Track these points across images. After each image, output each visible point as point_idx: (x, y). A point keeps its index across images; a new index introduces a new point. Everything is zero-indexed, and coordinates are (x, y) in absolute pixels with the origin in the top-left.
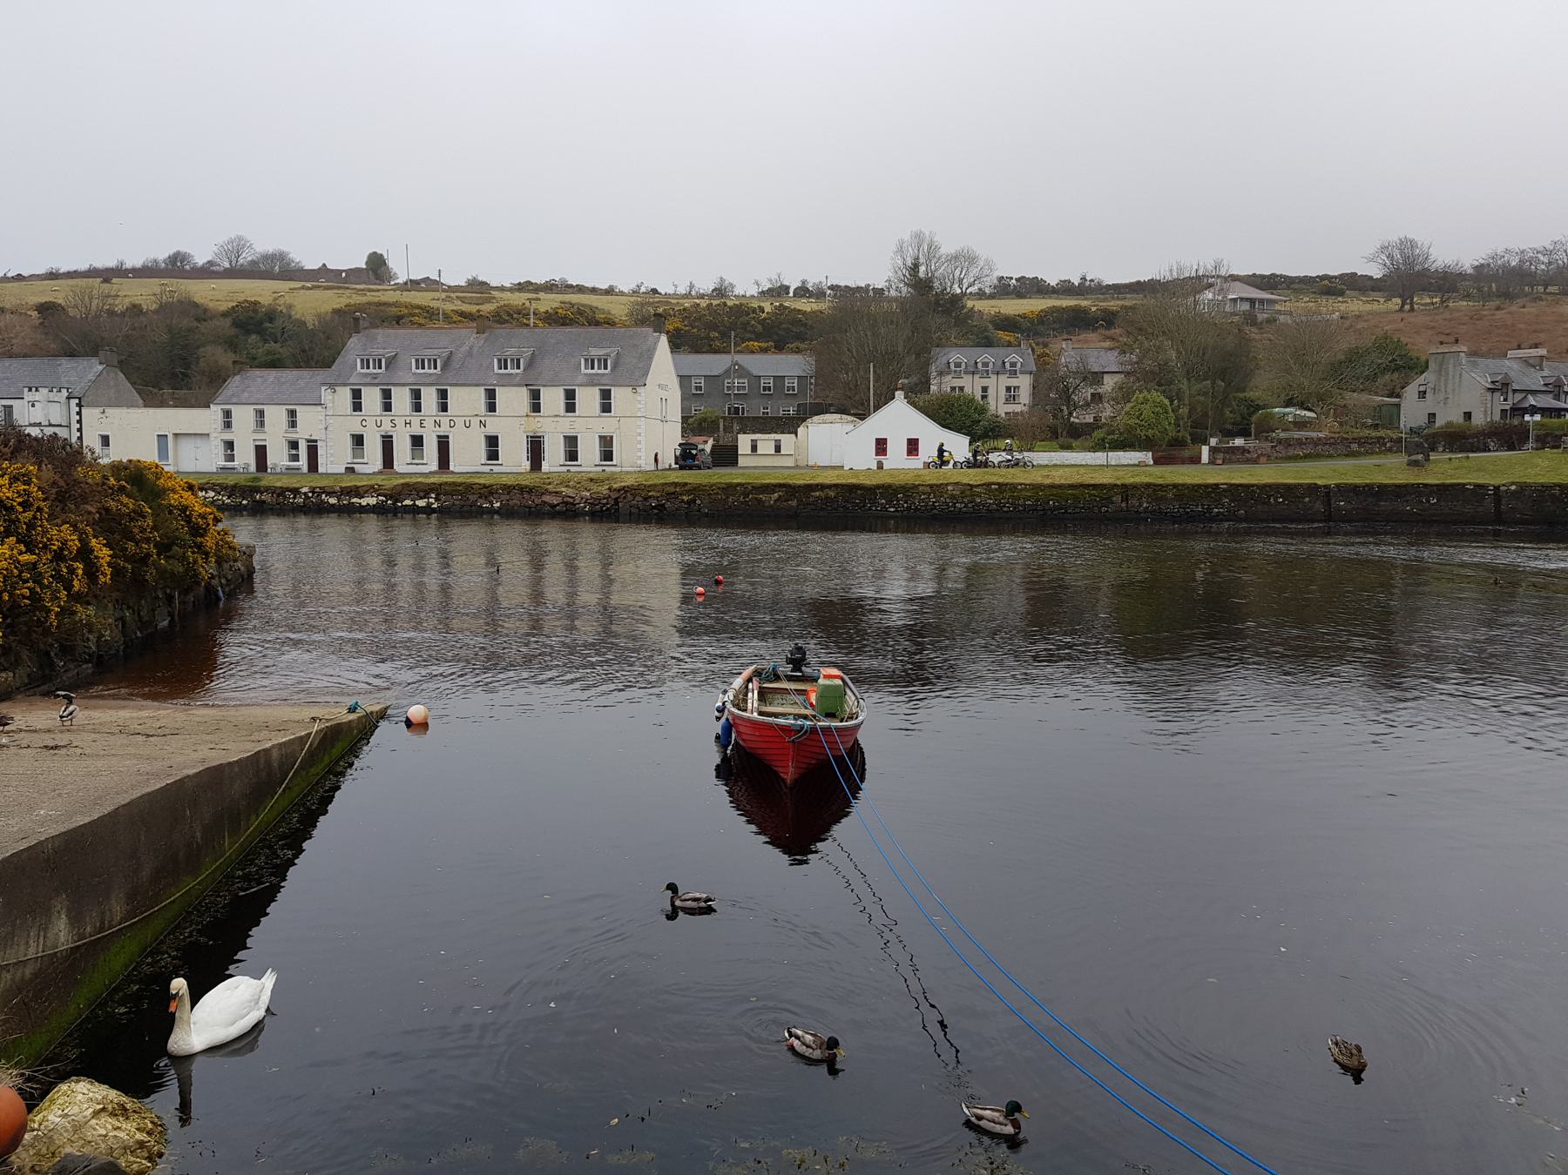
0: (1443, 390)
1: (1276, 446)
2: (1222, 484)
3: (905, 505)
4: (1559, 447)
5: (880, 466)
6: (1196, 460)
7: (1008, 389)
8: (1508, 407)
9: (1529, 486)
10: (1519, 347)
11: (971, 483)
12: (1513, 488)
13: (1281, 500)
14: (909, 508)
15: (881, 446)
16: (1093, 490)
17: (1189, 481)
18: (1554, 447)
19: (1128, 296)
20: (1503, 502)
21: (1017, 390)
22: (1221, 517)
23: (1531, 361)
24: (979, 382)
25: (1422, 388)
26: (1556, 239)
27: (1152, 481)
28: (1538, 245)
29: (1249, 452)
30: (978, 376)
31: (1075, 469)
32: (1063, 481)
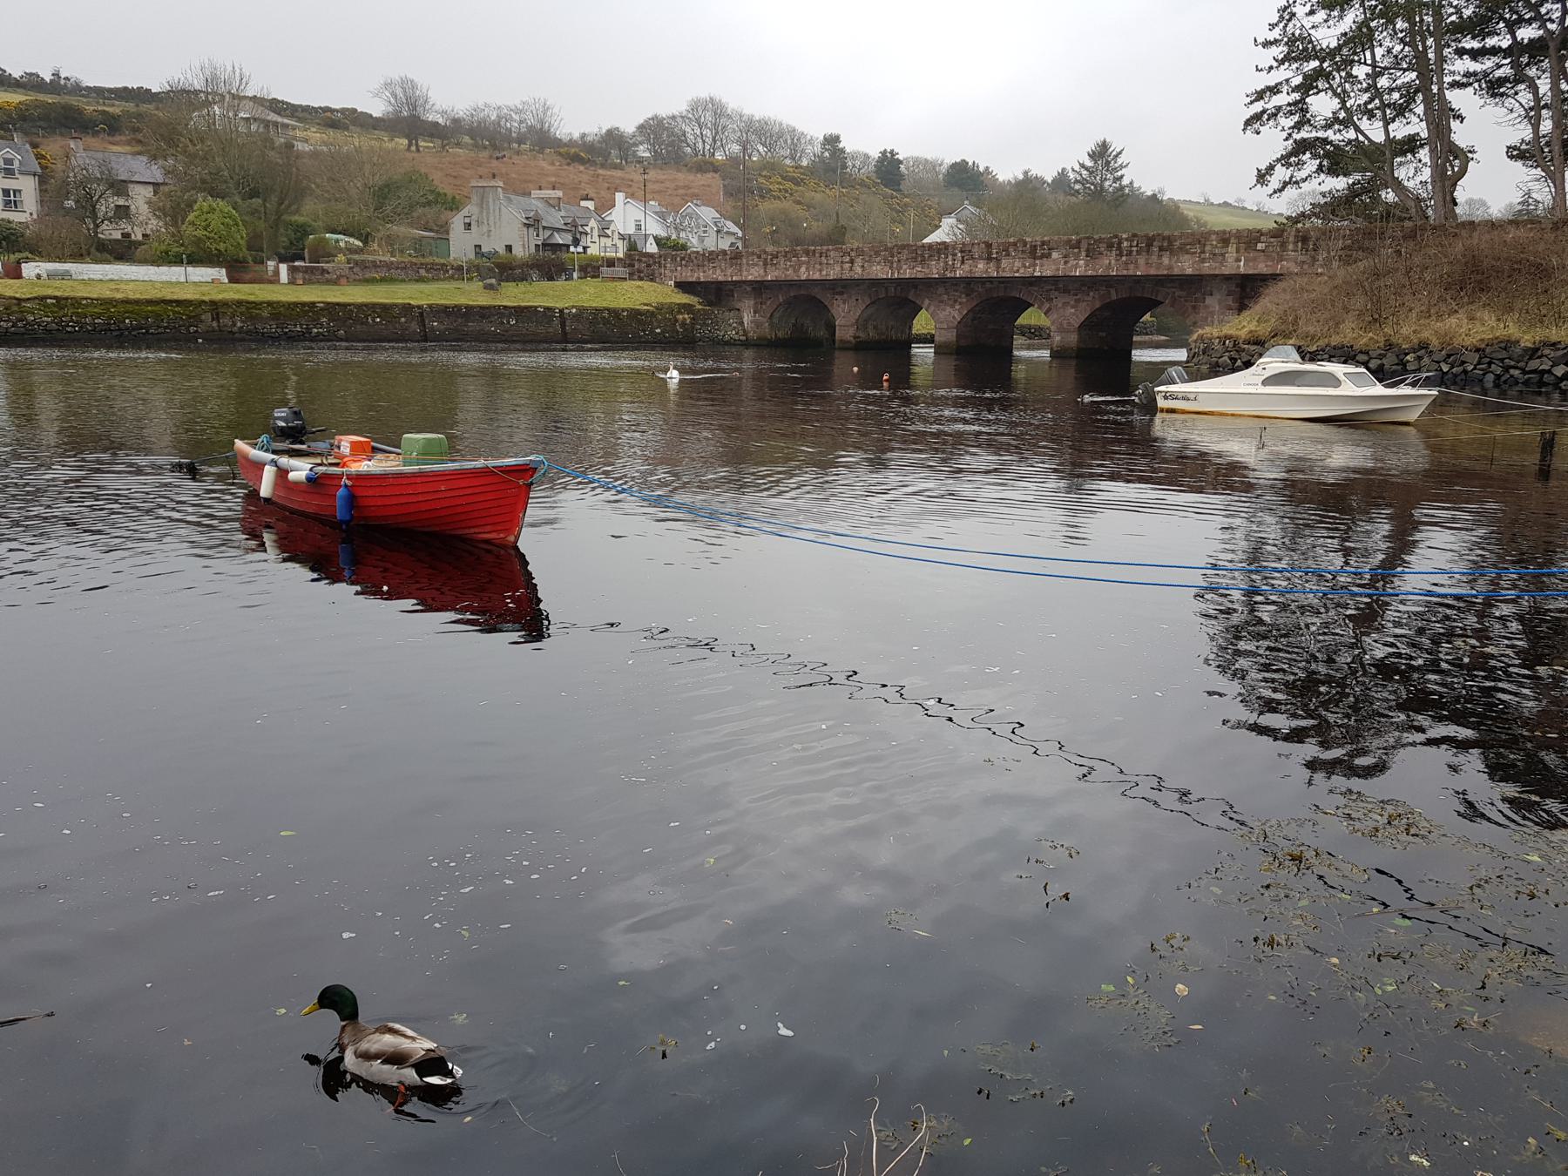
0: (485, 222)
1: (353, 268)
2: (319, 303)
4: (598, 276)
6: (275, 279)
8: (540, 243)
9: (585, 309)
10: (540, 188)
11: (17, 296)
12: (574, 311)
13: (378, 320)
16: (177, 306)
17: (283, 299)
18: (593, 277)
23: (551, 202)
25: (467, 220)
26: (524, 100)
27: (243, 297)
28: (511, 103)
29: (328, 273)
32: (138, 296)
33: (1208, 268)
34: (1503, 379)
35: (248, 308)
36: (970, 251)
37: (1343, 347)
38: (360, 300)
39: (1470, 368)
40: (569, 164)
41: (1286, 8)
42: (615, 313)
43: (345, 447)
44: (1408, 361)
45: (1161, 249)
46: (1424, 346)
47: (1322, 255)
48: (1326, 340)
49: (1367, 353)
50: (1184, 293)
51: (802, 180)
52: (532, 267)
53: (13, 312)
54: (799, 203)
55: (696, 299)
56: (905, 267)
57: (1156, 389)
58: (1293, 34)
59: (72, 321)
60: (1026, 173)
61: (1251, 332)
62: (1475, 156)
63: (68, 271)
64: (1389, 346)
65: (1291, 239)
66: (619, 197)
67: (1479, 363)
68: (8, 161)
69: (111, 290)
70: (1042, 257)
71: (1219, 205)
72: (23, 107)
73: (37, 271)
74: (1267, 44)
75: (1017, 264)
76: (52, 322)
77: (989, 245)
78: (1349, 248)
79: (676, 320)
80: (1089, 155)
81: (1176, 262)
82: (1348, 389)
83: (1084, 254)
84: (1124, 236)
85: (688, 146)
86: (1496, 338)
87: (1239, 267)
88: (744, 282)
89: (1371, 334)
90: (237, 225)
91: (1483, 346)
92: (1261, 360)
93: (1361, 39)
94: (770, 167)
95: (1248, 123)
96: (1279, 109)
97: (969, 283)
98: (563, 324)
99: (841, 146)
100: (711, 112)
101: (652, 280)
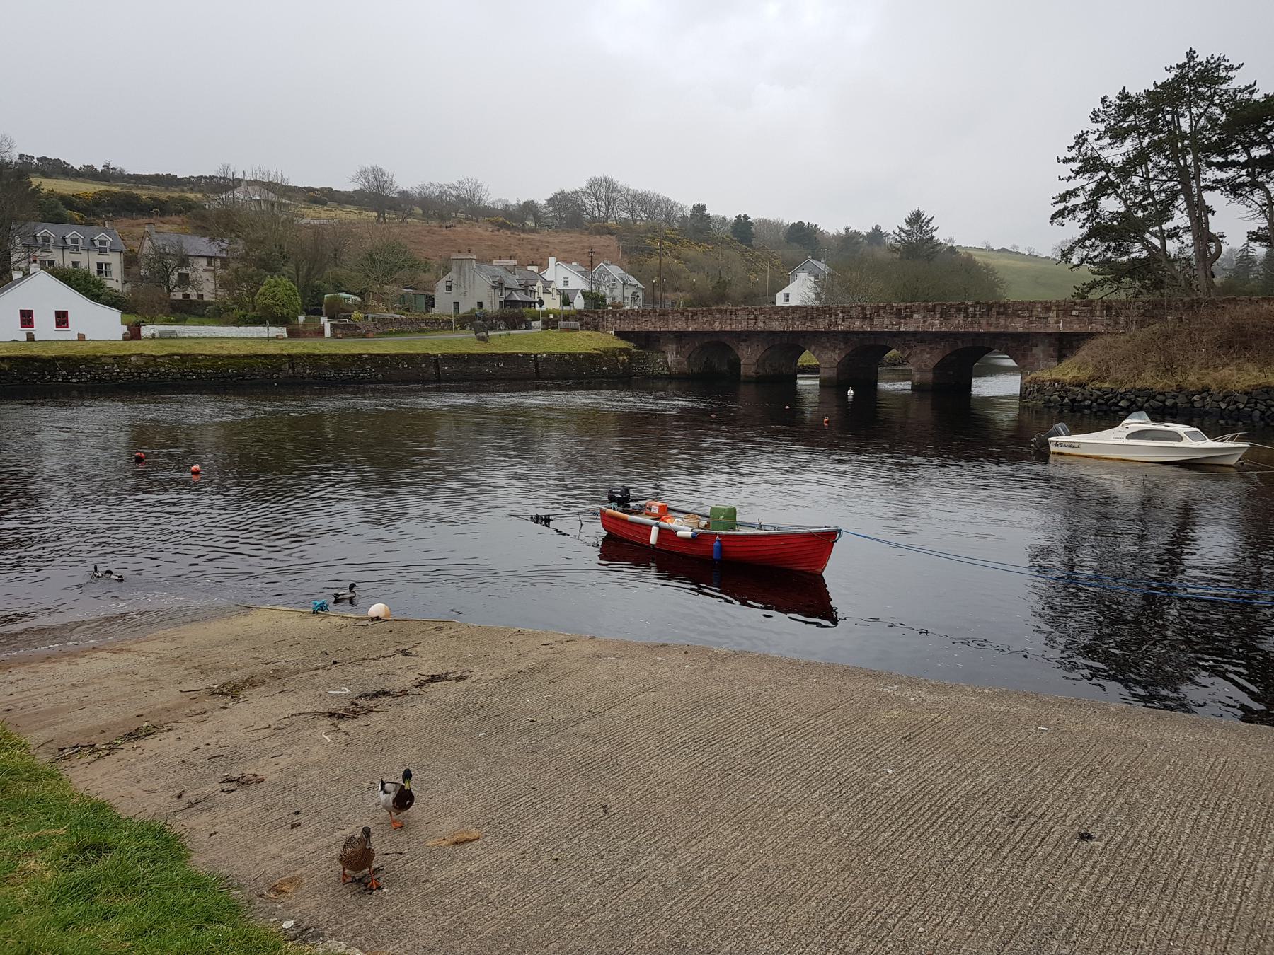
3: (89, 376)
4: (557, 328)
5: (30, 337)
6: (320, 333)
7: (100, 265)
8: (502, 300)
11: (153, 354)
14: (93, 379)
15: (27, 318)
18: (552, 328)
19: (151, 187)
20: (540, 364)
21: (108, 266)
22: (366, 380)
24: (95, 258)
25: (448, 284)
27: (311, 352)
30: (69, 251)
31: (243, 341)
32: (237, 352)
33: (1035, 327)
34: (1266, 415)
35: (315, 360)
36: (849, 312)
37: (1145, 389)
38: (393, 352)
39: (1242, 406)
40: (498, 230)
41: (1080, 136)
42: (573, 356)
43: (655, 509)
44: (1195, 401)
45: (998, 313)
46: (1206, 389)
47: (1122, 320)
48: (1132, 384)
49: (1163, 394)
50: (1015, 344)
51: (678, 240)
52: (498, 319)
53: (150, 366)
54: (677, 258)
55: (632, 344)
56: (797, 323)
57: (1050, 439)
58: (1086, 154)
59: (191, 372)
60: (847, 229)
61: (1074, 377)
62: (1224, 240)
63: (174, 331)
64: (1180, 389)
65: (1098, 308)
66: (552, 260)
67: (1248, 403)
69: (217, 348)
70: (906, 317)
71: (998, 250)
72: (97, 197)
73: (152, 332)
74: (1066, 161)
75: (886, 322)
76: (178, 372)
77: (863, 308)
78: (1143, 315)
79: (618, 361)
80: (906, 221)
81: (1010, 323)
82: (1187, 443)
83: (938, 316)
84: (969, 303)
85: (587, 213)
86: (1260, 384)
87: (1059, 327)
88: (668, 332)
89: (1166, 381)
90: (295, 295)
91: (1250, 390)
92: (1124, 422)
93: (1140, 158)
94: (654, 230)
95: (1054, 217)
96: (1076, 206)
97: (846, 336)
98: (537, 365)
99: (706, 213)
100: (606, 189)
101: (597, 330)
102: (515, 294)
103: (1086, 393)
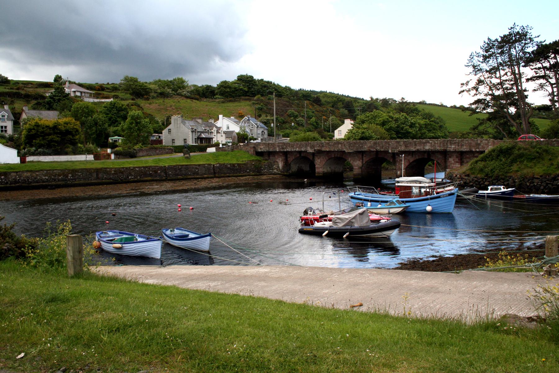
39: (536, 184)
60: (372, 98)
66: (221, 116)
68: (3, 116)
102: (202, 134)
103: (471, 179)
